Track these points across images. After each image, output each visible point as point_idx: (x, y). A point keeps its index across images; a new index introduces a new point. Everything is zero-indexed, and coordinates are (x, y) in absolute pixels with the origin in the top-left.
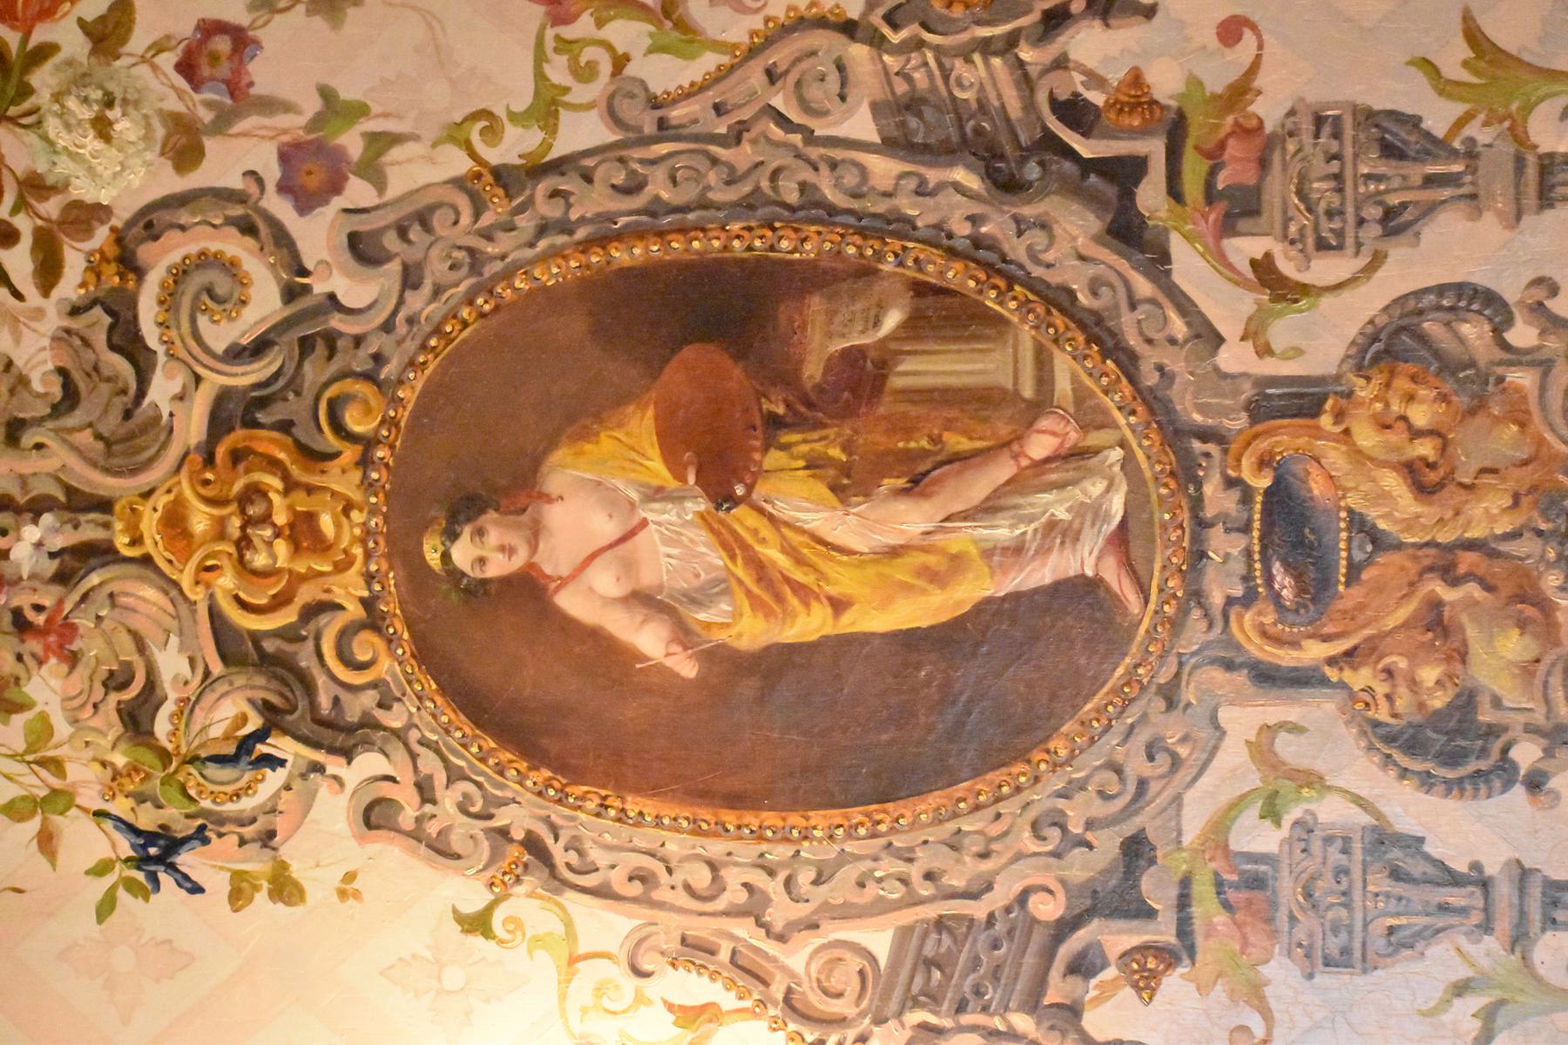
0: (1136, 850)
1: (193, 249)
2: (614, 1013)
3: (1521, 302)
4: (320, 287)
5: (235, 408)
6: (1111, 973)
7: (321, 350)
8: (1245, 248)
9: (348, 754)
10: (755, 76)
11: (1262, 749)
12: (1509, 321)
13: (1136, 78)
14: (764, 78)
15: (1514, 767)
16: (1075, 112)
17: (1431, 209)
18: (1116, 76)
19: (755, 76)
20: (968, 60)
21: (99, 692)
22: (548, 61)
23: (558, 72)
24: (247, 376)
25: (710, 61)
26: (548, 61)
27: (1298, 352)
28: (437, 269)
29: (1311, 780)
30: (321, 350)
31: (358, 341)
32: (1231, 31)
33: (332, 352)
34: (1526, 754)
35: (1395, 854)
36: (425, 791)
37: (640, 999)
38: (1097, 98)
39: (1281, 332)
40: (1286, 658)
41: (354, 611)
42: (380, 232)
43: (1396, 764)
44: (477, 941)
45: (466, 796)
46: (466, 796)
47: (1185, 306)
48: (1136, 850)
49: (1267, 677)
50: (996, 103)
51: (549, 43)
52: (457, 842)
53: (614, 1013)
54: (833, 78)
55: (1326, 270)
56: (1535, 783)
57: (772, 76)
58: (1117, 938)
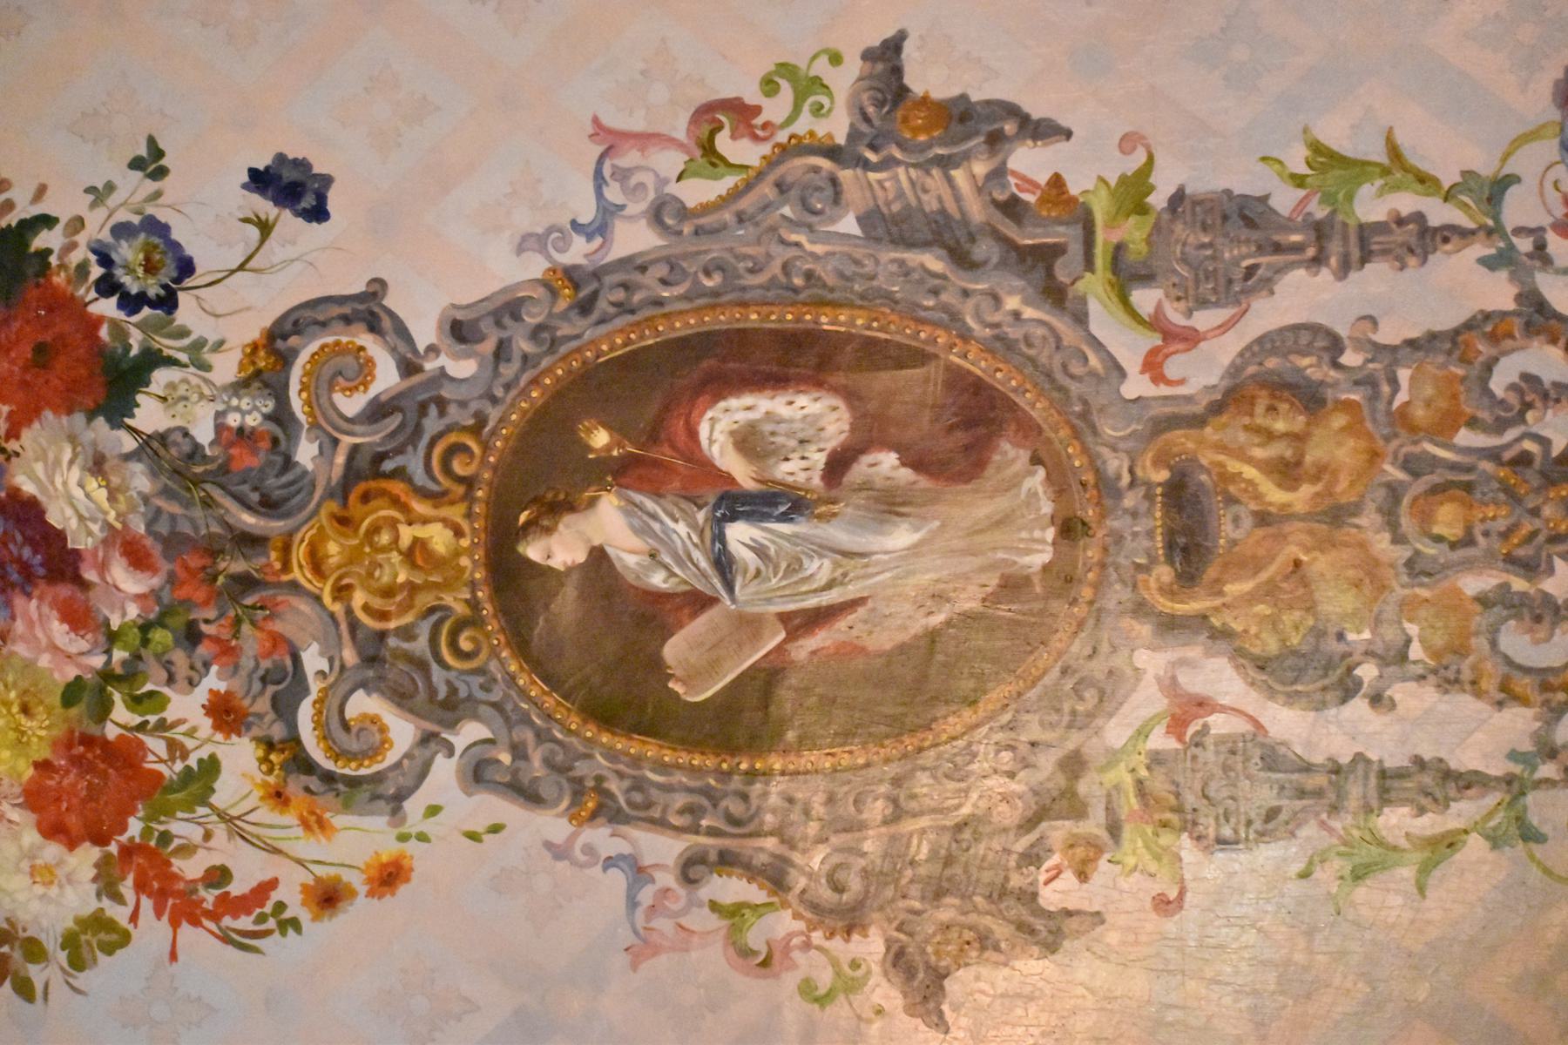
0: (1074, 764)
1: (330, 340)
2: (1548, 169)
3: (1349, 338)
4: (430, 366)
5: (363, 462)
6: (1055, 859)
7: (433, 410)
8: (1145, 299)
9: (452, 725)
10: (767, 190)
11: (1170, 686)
12: (1341, 351)
13: (1057, 182)
14: (776, 190)
15: (1359, 683)
16: (1012, 208)
17: (1281, 270)
18: (1043, 178)
19: (767, 190)
20: (928, 173)
21: (257, 686)
22: (607, 185)
23: (613, 193)
24: (369, 438)
25: (729, 182)
26: (607, 185)
27: (1182, 382)
28: (524, 345)
29: (1203, 705)
30: (433, 410)
31: (463, 404)
32: (1128, 143)
33: (442, 413)
34: (1367, 672)
35: (1091, 622)
36: (519, 751)
37: (692, 903)
38: (1029, 198)
39: (1172, 369)
40: (1181, 608)
41: (460, 609)
42: (477, 320)
43: (1278, 692)
44: (562, 866)
45: (552, 751)
46: (552, 751)
47: (1098, 345)
48: (1074, 764)
49: (1170, 625)
50: (957, 216)
51: (607, 171)
52: (546, 791)
53: (1548, 169)
54: (829, 192)
55: (1204, 320)
56: (1376, 700)
57: (781, 187)
58: (1057, 831)
